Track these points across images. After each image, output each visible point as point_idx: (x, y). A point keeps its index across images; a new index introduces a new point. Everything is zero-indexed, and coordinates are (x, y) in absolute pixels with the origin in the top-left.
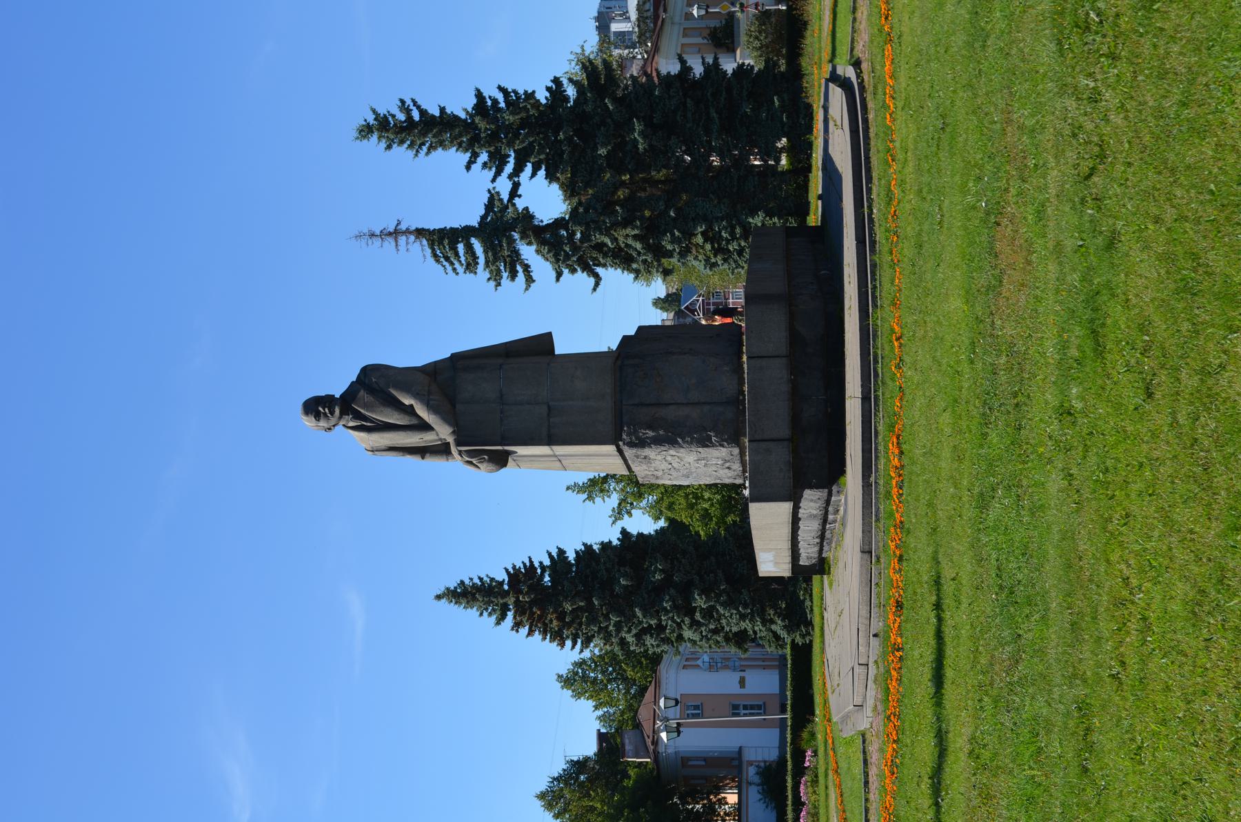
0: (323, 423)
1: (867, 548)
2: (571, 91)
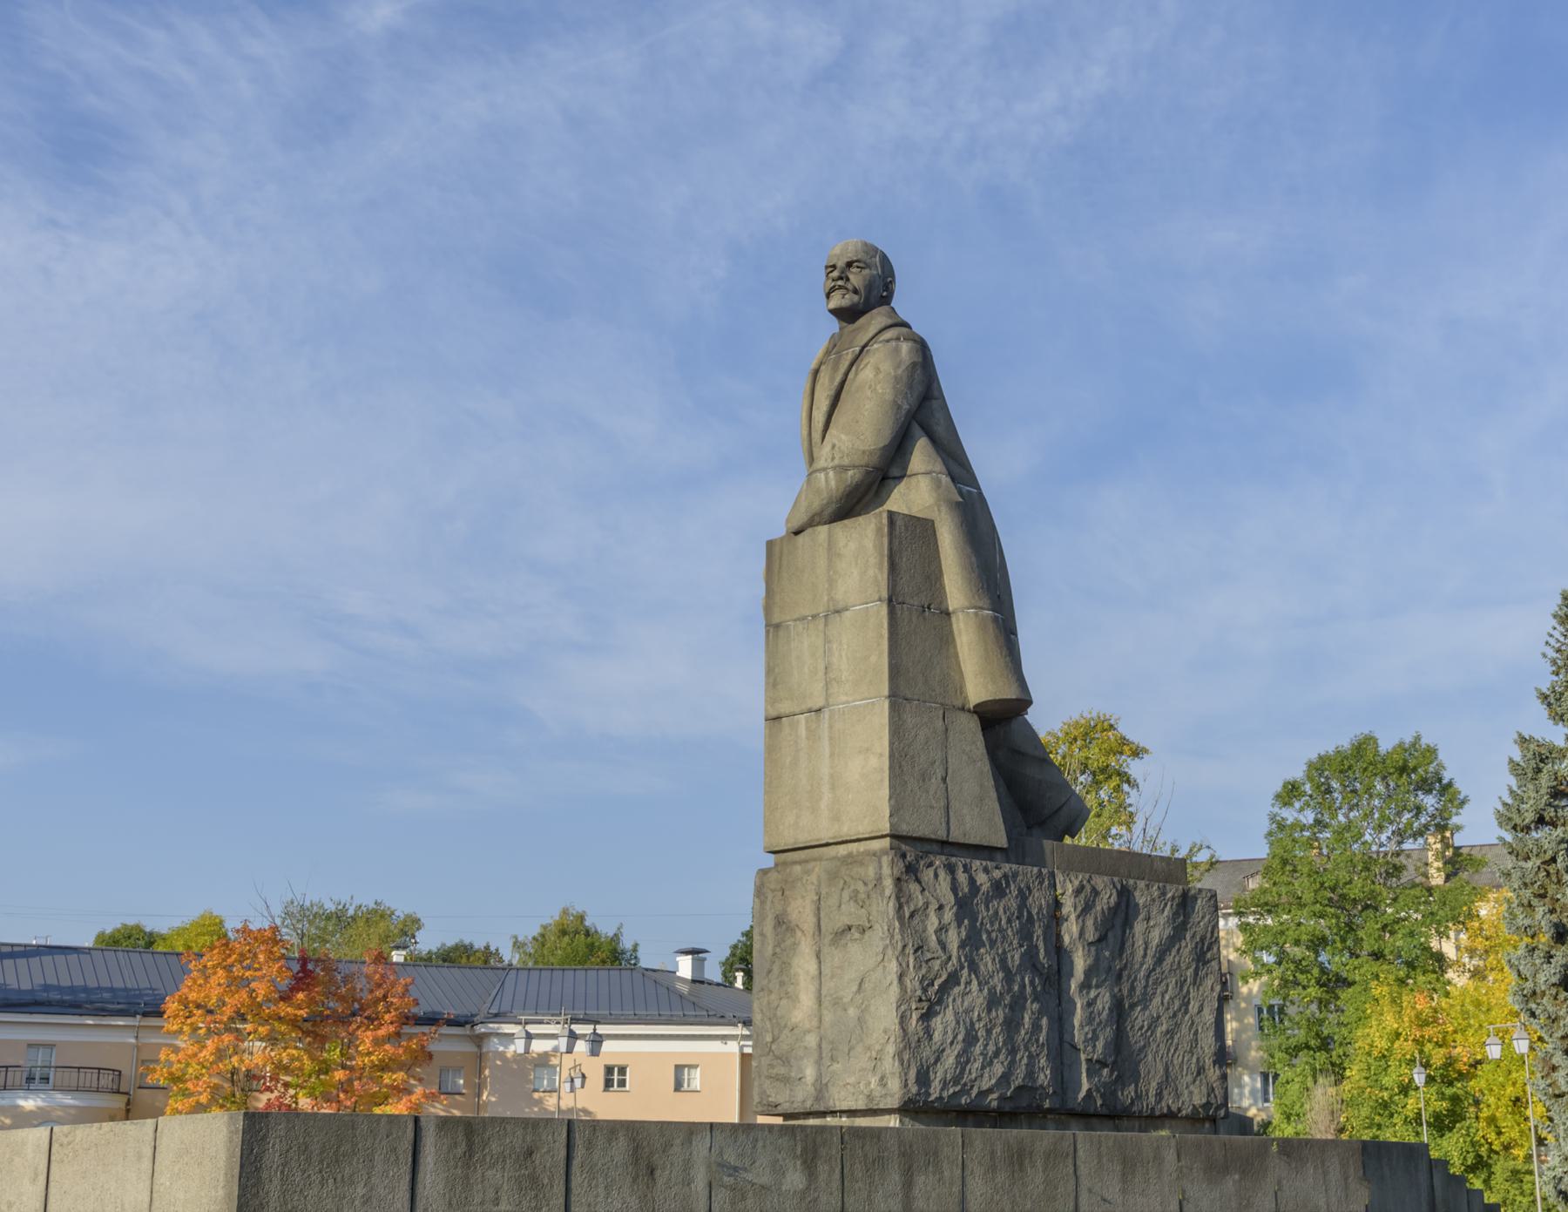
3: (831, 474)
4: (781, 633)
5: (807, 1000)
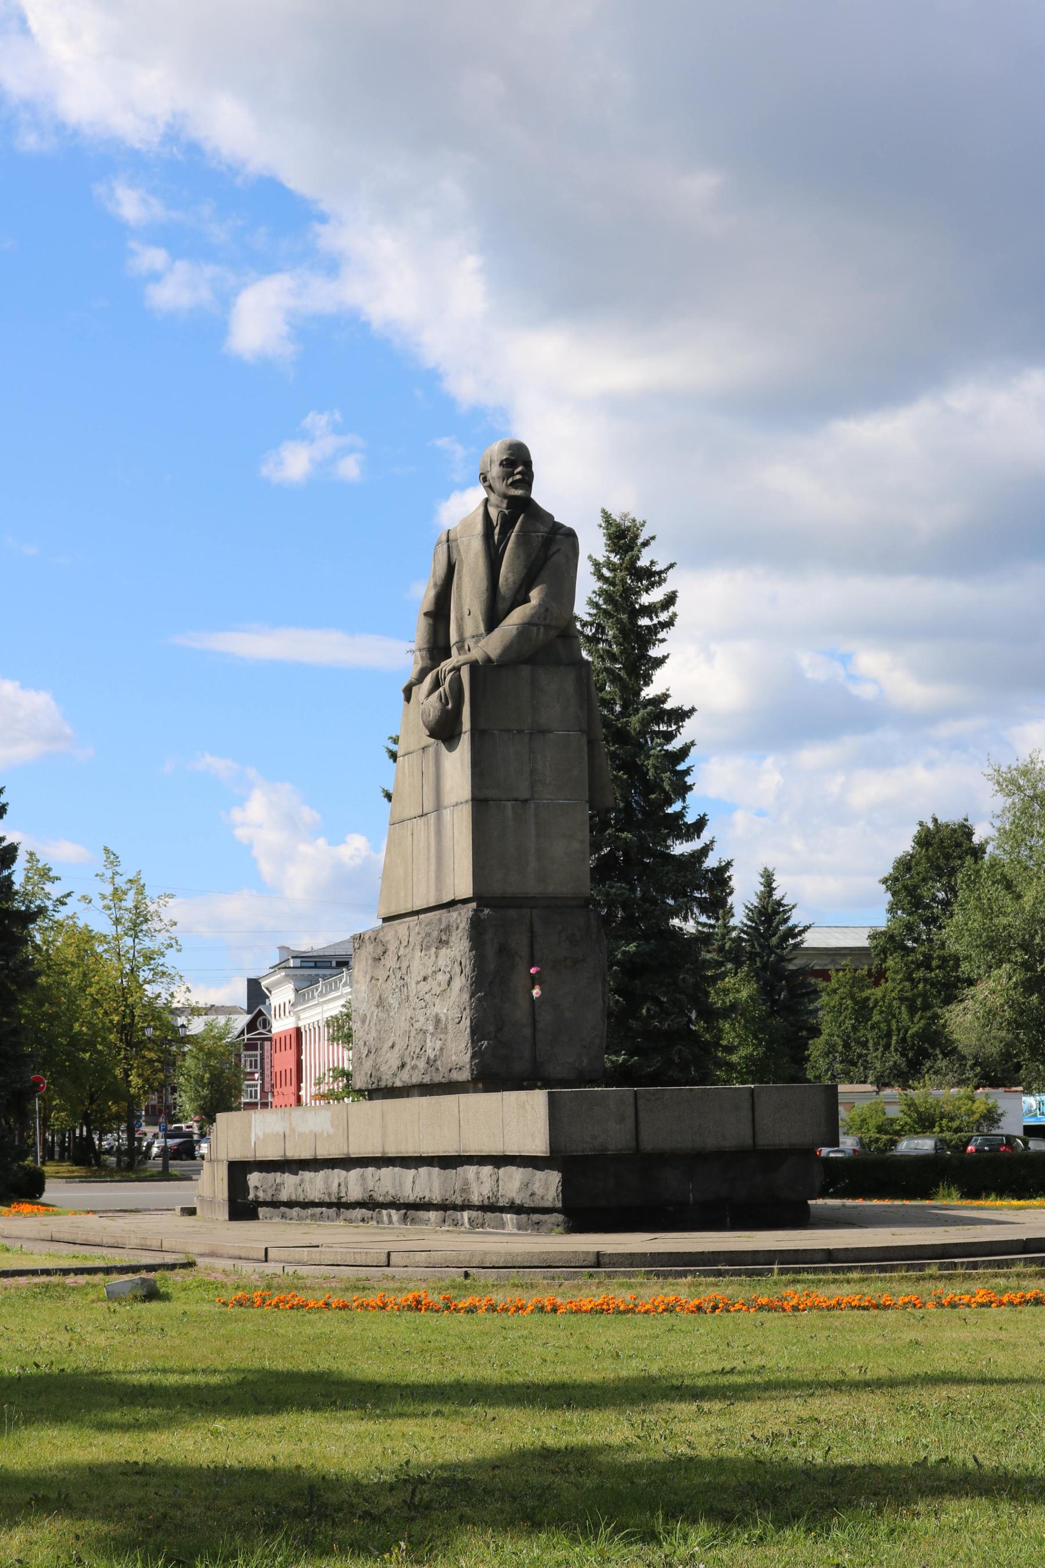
0: (495, 471)
1: (603, 1260)
2: (680, 848)
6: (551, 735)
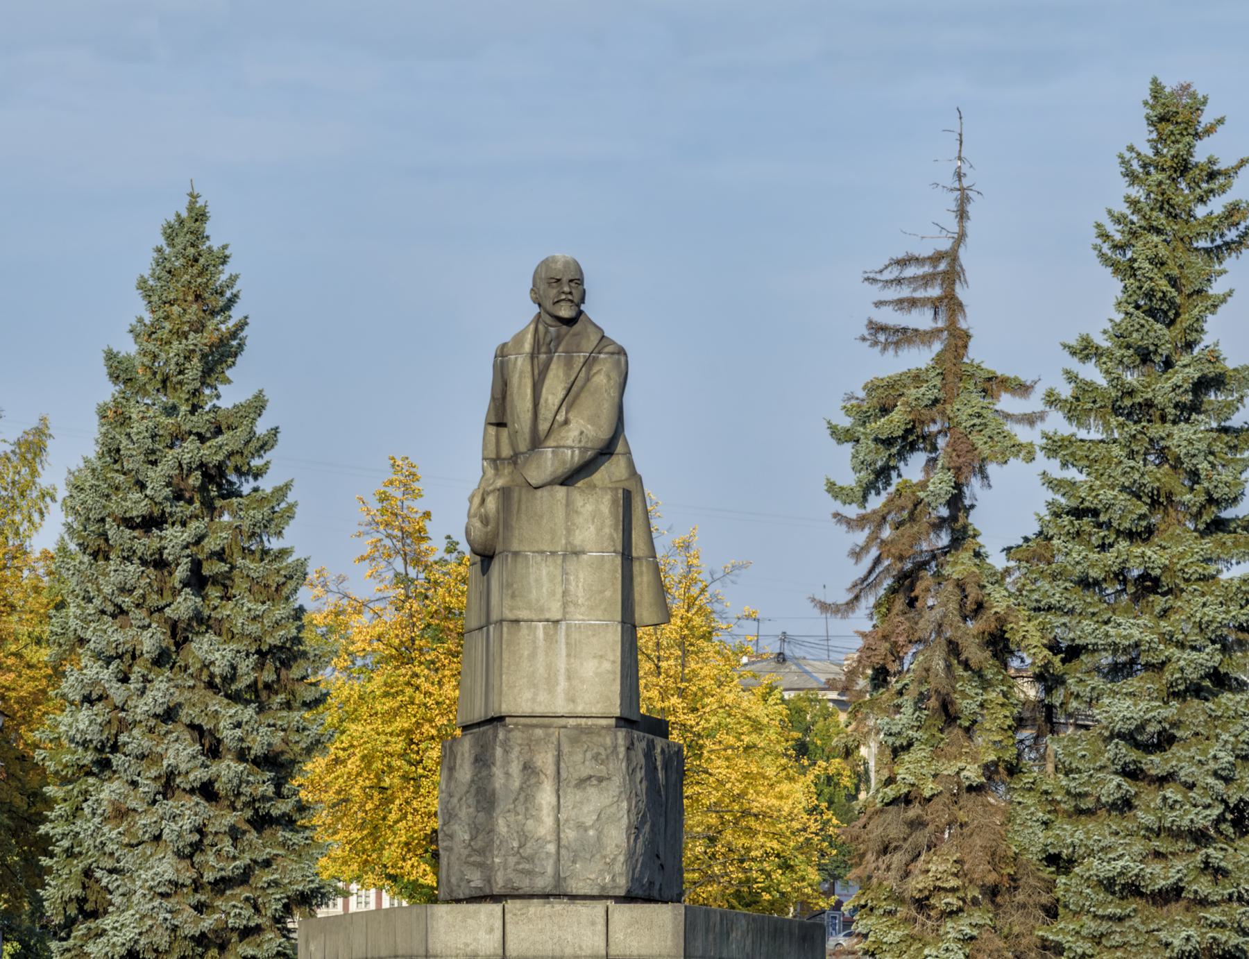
3: (577, 452)
4: (520, 559)
5: (549, 821)
6: (585, 557)
